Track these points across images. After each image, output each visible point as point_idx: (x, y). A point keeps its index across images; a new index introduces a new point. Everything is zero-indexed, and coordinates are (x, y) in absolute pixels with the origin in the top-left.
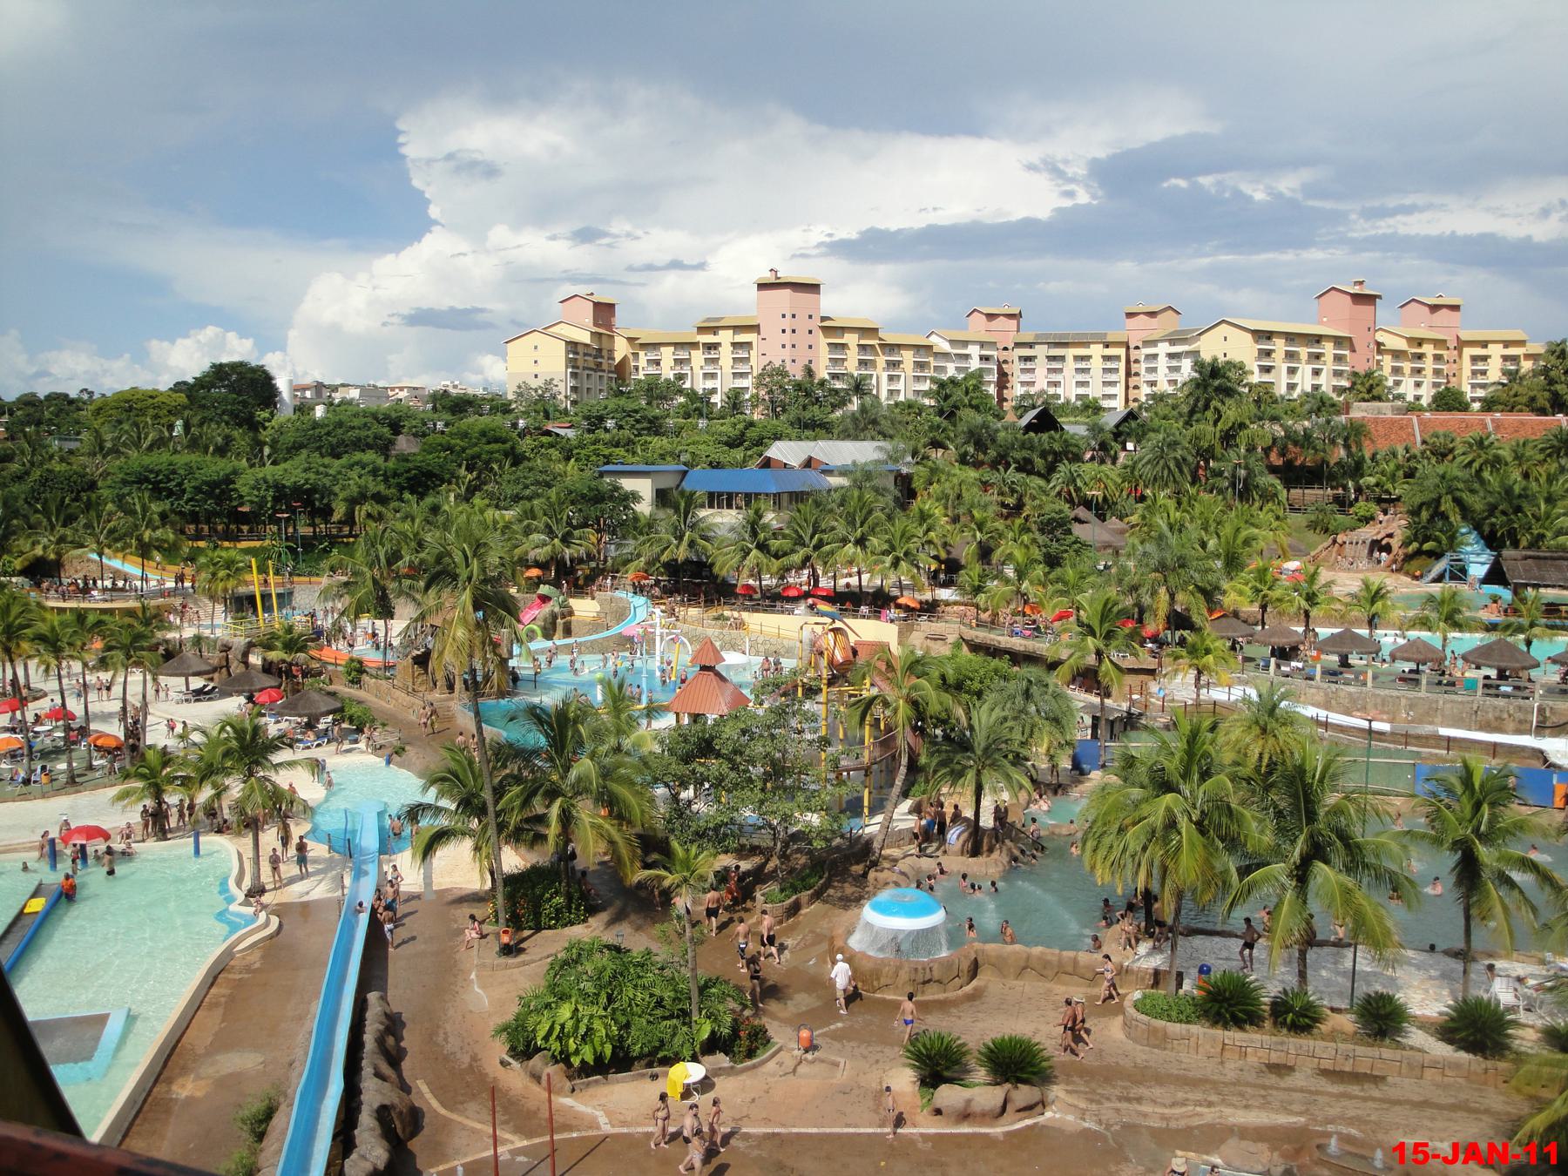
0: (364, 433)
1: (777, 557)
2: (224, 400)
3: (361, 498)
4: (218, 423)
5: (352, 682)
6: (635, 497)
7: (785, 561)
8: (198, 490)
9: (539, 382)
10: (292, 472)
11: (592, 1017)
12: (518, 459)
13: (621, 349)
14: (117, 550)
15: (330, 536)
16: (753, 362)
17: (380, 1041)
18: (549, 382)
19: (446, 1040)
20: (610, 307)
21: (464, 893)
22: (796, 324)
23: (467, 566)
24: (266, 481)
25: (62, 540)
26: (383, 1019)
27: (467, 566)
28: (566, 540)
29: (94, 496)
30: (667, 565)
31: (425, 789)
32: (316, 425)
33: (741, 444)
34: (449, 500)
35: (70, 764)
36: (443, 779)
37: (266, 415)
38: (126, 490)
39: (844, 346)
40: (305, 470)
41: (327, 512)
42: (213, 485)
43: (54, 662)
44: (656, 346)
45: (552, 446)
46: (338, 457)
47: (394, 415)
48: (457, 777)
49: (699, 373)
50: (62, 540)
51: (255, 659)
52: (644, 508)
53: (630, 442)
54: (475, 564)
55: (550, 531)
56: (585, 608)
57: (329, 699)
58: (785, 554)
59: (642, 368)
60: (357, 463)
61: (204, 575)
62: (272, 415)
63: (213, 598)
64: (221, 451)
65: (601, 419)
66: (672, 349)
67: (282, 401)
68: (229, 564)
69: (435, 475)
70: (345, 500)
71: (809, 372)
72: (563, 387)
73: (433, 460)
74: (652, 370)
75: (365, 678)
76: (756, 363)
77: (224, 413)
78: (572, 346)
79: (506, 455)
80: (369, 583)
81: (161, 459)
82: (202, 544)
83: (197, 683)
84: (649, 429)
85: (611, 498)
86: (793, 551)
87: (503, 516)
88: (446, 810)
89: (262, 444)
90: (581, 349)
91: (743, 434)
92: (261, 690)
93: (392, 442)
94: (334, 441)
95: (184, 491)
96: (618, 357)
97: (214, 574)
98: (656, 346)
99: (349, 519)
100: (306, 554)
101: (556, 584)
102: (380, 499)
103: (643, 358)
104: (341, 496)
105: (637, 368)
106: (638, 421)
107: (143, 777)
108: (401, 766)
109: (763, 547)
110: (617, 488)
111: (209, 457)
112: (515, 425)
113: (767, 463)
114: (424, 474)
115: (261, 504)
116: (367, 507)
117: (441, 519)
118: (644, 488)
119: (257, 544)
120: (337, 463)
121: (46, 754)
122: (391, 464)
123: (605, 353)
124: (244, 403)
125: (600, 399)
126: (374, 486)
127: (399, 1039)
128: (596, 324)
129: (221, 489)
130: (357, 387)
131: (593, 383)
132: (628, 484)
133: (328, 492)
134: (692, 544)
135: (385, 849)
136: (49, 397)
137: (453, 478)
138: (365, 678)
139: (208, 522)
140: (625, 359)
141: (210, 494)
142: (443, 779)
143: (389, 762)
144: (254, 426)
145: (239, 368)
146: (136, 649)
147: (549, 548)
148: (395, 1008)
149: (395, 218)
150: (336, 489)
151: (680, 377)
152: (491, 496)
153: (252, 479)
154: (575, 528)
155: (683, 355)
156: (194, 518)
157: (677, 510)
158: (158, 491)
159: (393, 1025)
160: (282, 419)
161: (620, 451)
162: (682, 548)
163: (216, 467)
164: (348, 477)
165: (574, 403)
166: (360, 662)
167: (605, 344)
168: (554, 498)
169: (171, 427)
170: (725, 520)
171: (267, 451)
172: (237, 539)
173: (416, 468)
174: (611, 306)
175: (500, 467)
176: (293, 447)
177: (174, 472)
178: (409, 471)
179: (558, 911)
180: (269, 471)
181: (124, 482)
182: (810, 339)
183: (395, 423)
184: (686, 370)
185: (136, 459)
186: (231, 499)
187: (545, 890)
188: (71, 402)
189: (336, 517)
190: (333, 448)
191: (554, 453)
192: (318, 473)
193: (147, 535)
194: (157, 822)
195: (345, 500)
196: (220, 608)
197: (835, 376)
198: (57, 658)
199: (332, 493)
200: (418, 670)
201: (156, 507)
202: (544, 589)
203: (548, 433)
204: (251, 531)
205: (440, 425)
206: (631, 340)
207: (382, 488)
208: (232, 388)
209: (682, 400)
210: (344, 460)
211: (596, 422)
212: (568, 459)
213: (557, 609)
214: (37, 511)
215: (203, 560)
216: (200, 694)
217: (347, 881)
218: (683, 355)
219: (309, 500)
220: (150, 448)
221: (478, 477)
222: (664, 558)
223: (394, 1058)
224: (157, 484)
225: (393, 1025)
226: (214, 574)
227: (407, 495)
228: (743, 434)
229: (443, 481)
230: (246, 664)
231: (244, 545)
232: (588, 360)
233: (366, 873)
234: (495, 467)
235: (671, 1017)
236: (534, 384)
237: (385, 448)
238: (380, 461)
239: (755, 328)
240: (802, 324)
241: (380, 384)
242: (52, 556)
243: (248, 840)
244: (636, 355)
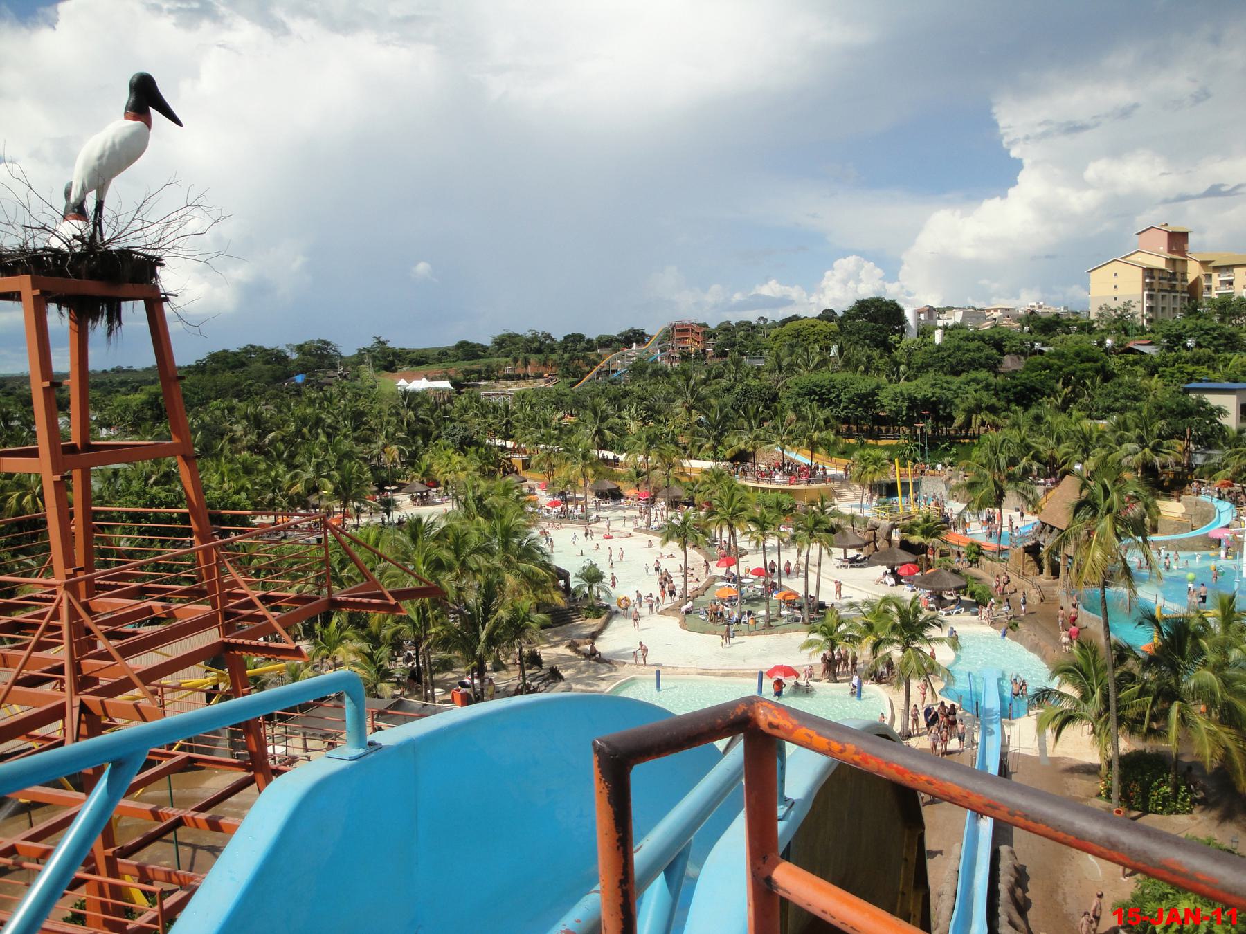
0: (977, 355)
3: (978, 408)
4: (862, 346)
6: (1220, 411)
8: (851, 400)
9: (1119, 304)
10: (922, 387)
12: (1108, 376)
13: (1194, 271)
14: (794, 447)
15: (949, 436)
17: (1012, 892)
19: (1064, 900)
20: (1184, 236)
21: (1074, 764)
24: (902, 394)
25: (757, 437)
26: (1013, 872)
28: (1156, 450)
29: (779, 406)
31: (1052, 677)
32: (940, 348)
34: (1046, 407)
35: (768, 612)
36: (1069, 671)
37: (896, 338)
38: (800, 400)
40: (932, 386)
41: (950, 419)
42: (862, 397)
43: (761, 538)
44: (1229, 268)
45: (1136, 363)
46: (957, 374)
47: (997, 337)
48: (1081, 670)
50: (757, 437)
51: (896, 536)
52: (1231, 421)
53: (1210, 359)
54: (1115, 497)
55: (1141, 440)
56: (1171, 509)
57: (954, 577)
59: (1216, 288)
60: (973, 380)
61: (858, 469)
62: (901, 338)
63: (863, 486)
65: (1180, 337)
67: (909, 326)
68: (876, 461)
69: (1038, 390)
70: (964, 410)
73: (1035, 377)
74: (1225, 290)
75: (982, 559)
77: (865, 338)
78: (1149, 272)
79: (1097, 372)
80: (992, 485)
81: (823, 376)
82: (852, 441)
83: (852, 553)
84: (1225, 345)
85: (1198, 413)
87: (1096, 425)
88: (1069, 696)
89: (897, 364)
90: (1156, 274)
92: (902, 564)
93: (1000, 362)
95: (840, 401)
96: (1191, 278)
97: (864, 468)
98: (1229, 268)
99: (968, 424)
102: (992, 409)
103: (1216, 279)
104: (962, 407)
105: (1209, 288)
106: (1215, 338)
107: (823, 633)
108: (1014, 639)
110: (1204, 404)
111: (858, 375)
112: (1101, 343)
114: (1027, 389)
115: (898, 412)
116: (983, 416)
117: (1044, 427)
119: (894, 442)
121: (750, 600)
122: (999, 380)
123: (1179, 276)
124: (881, 330)
125: (1177, 319)
126: (988, 399)
127: (1025, 890)
128: (1170, 251)
129: (868, 400)
130: (960, 309)
131: (1168, 303)
132: (1214, 400)
133: (949, 403)
135: (1007, 714)
136: (739, 325)
137: (1054, 392)
138: (982, 559)
139: (856, 423)
141: (859, 404)
142: (1069, 671)
143: (1004, 635)
144: (888, 348)
146: (818, 531)
147: (1140, 455)
148: (1021, 861)
149: (994, 173)
150: (957, 401)
152: (1084, 408)
154: (1164, 438)
156: (846, 420)
158: (823, 401)
159: (1021, 877)
160: (909, 341)
161: (1203, 369)
164: (966, 391)
165: (1150, 321)
166: (979, 546)
167: (1179, 268)
168: (1145, 413)
169: (828, 349)
171: (902, 368)
172: (877, 438)
173: (1022, 384)
175: (1093, 383)
176: (922, 367)
177: (834, 387)
178: (1016, 386)
179: (1165, 799)
180: (903, 386)
181: (798, 394)
183: (999, 343)
185: (806, 377)
187: (1155, 778)
188: (753, 327)
189: (957, 423)
190: (952, 367)
191: (1140, 370)
192: (942, 388)
193: (816, 436)
194: (832, 667)
195: (964, 410)
196: (867, 491)
198: (763, 535)
199: (953, 403)
200: (1028, 558)
201: (821, 415)
203: (1131, 351)
204: (888, 431)
205: (1037, 346)
206: (1204, 263)
207: (994, 400)
208: (872, 318)
210: (963, 377)
211: (1176, 340)
212: (1152, 375)
214: (740, 416)
215: (856, 455)
216: (854, 562)
219: (935, 409)
220: (816, 367)
221: (1073, 391)
223: (1022, 907)
224: (821, 396)
225: (1021, 877)
226: (864, 468)
227: (1013, 407)
229: (1043, 395)
230: (889, 541)
231: (882, 443)
232: (1161, 283)
233: (992, 732)
234: (1088, 382)
236: (1114, 305)
237: (993, 367)
238: (992, 379)
241: (978, 307)
242: (751, 449)
244: (1209, 277)
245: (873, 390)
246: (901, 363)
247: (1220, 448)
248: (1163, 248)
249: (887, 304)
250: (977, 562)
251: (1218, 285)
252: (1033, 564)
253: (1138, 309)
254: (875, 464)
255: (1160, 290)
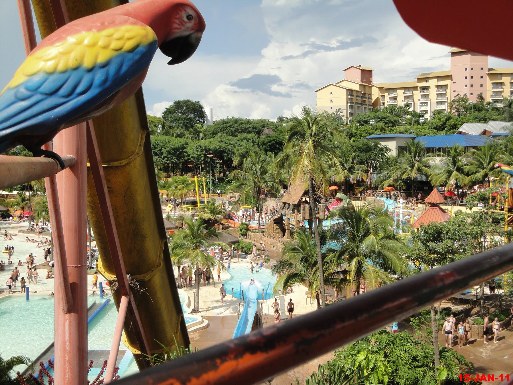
1: (468, 175)
2: (181, 118)
5: (242, 235)
7: (473, 177)
8: (169, 152)
10: (214, 143)
11: (376, 360)
13: (375, 94)
16: (448, 95)
18: (338, 110)
22: (473, 73)
23: (310, 128)
24: (201, 147)
27: (310, 128)
28: (351, 170)
30: (405, 182)
33: (444, 129)
39: (502, 84)
42: (176, 149)
44: (394, 90)
49: (418, 103)
58: (473, 173)
59: (388, 101)
60: (245, 139)
64: (180, 136)
66: (403, 91)
67: (207, 119)
71: (481, 97)
72: (345, 114)
74: (392, 103)
75: (249, 233)
76: (450, 96)
78: (350, 92)
86: (477, 172)
90: (354, 93)
91: (445, 124)
94: (233, 130)
98: (394, 90)
100: (220, 183)
101: (345, 192)
103: (387, 96)
105: (384, 103)
109: (459, 170)
111: (174, 138)
113: (460, 133)
118: (392, 145)
120: (235, 138)
123: (367, 95)
128: (362, 81)
134: (419, 170)
140: (378, 99)
141: (174, 154)
145: (187, 103)
150: (235, 150)
151: (408, 105)
153: (193, 148)
155: (409, 94)
157: (410, 153)
162: (414, 172)
163: (177, 142)
164: (238, 145)
167: (367, 91)
170: (437, 161)
173: (274, 140)
174: (370, 72)
177: (158, 144)
178: (270, 142)
180: (203, 143)
182: (481, 81)
184: (410, 102)
186: (184, 157)
192: (226, 143)
197: (496, 101)
202: (339, 195)
206: (380, 89)
209: (408, 117)
213: (346, 205)
217: (242, 309)
218: (409, 94)
222: (404, 176)
228: (445, 124)
232: (358, 99)
235: (421, 367)
236: (331, 112)
237: (259, 133)
239: (450, 77)
240: (477, 69)
243: (194, 291)
244: (383, 97)
245: (183, 145)
246: (200, 132)
247: (387, 169)
248: (358, 79)
249: (194, 104)
250: (246, 235)
251: (389, 100)
252: (279, 230)
253: (344, 113)
254: (183, 184)
255: (357, 103)
